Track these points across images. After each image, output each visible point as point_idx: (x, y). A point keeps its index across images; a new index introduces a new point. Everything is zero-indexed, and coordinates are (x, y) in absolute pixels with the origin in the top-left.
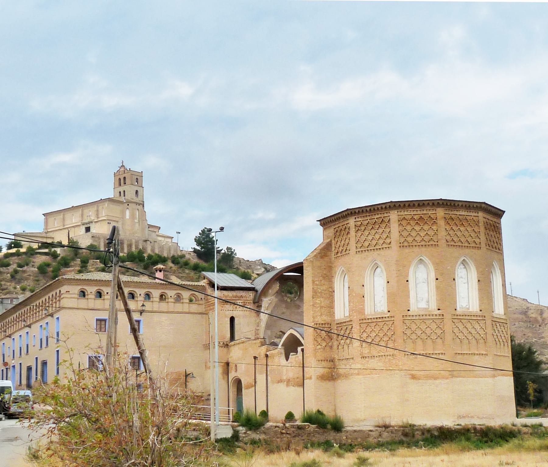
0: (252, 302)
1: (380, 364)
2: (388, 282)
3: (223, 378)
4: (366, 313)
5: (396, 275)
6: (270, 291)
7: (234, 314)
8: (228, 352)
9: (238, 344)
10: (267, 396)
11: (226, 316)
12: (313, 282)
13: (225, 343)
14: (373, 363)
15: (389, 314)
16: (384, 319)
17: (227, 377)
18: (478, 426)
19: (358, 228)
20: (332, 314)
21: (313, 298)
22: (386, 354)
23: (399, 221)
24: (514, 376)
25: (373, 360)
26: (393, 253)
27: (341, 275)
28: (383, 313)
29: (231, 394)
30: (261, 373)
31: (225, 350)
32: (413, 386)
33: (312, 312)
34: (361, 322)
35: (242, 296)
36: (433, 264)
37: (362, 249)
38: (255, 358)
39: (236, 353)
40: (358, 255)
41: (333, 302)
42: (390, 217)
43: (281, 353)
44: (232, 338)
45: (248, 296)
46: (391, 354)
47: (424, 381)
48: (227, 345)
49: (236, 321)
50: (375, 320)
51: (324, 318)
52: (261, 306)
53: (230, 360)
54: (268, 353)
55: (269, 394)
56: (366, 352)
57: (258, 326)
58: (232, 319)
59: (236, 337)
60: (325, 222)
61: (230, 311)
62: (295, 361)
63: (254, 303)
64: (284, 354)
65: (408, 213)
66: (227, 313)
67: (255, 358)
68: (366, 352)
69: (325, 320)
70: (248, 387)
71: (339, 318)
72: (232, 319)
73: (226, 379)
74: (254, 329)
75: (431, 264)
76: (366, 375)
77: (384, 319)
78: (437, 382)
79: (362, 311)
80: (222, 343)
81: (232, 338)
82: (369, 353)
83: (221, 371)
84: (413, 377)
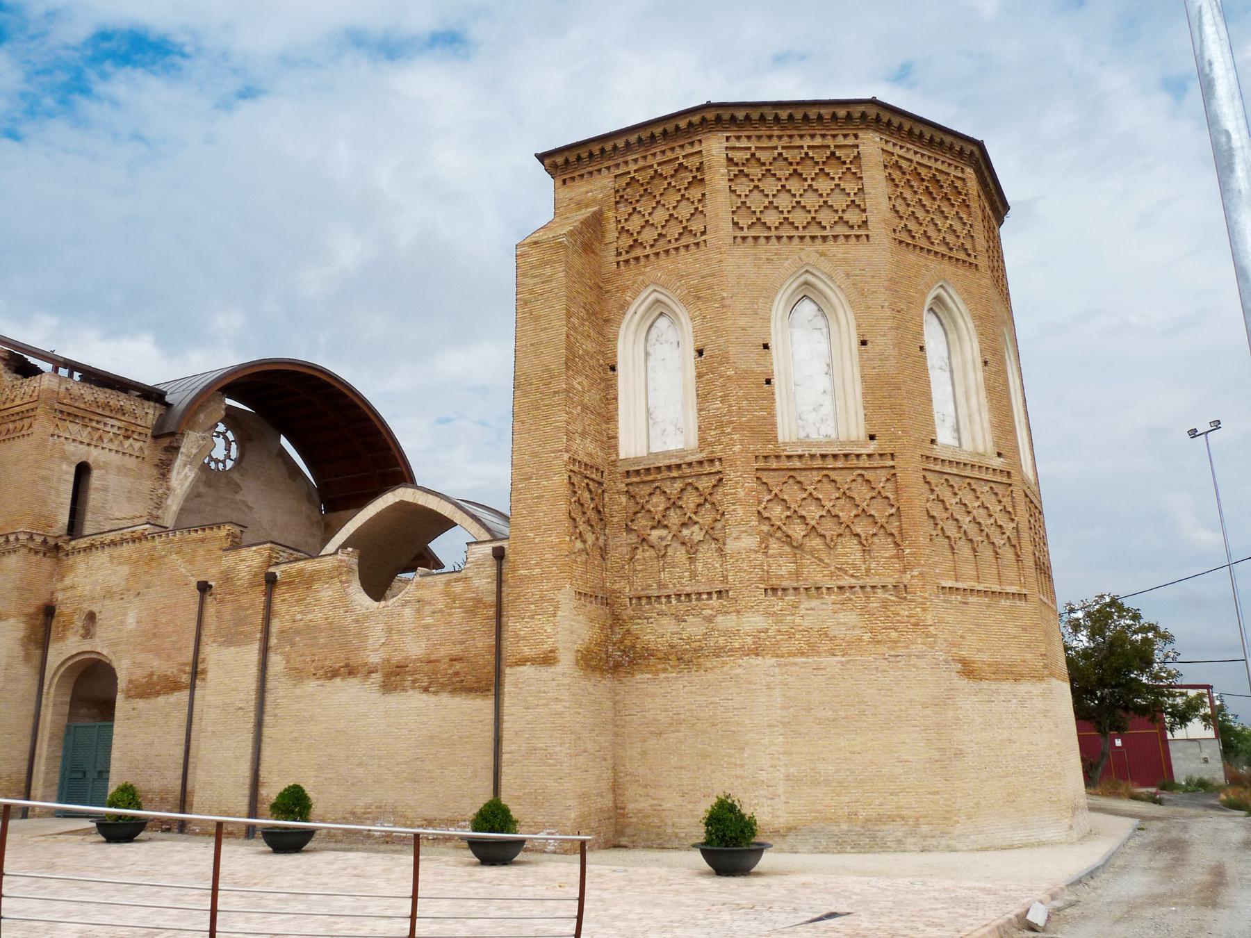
0: (149, 432)
1: (850, 618)
2: (864, 343)
3: (27, 658)
4: (780, 439)
5: (890, 323)
6: (202, 417)
7: (94, 455)
8: (60, 572)
9: (113, 543)
10: (259, 724)
11: (65, 457)
12: (569, 315)
13: (51, 542)
14: (816, 614)
15: (872, 447)
16: (854, 462)
17: (38, 652)
18: (1049, 834)
19: (738, 171)
20: (610, 441)
21: (568, 368)
22: (869, 581)
23: (886, 166)
24: (1072, 681)
25: (814, 603)
26: (878, 253)
27: (642, 317)
28: (855, 443)
29: (48, 715)
30: (231, 639)
31: (47, 563)
32: (970, 700)
33: (564, 417)
34: (761, 464)
35: (122, 410)
36: (974, 317)
37: (753, 229)
38: (204, 587)
39: (91, 577)
40: (740, 250)
41: (609, 398)
42: (861, 148)
43: (350, 570)
44: (74, 527)
45: (139, 412)
46: (890, 581)
47: (994, 686)
48: (57, 548)
49: (95, 479)
50: (818, 463)
51: (591, 447)
52: (177, 449)
53: (60, 596)
54: (277, 571)
55: (268, 719)
56: (784, 571)
57: (158, 506)
58: (83, 471)
59: (89, 527)
60: (564, 162)
61: (76, 445)
62: (447, 593)
63: (156, 437)
64: (357, 574)
65: (910, 153)
66: (70, 447)
67: (204, 587)
68: (784, 571)
69: (590, 455)
70: (149, 689)
71: (641, 452)
72: (83, 471)
73: (36, 661)
74: (145, 513)
75: (968, 318)
76: (791, 654)
77: (854, 462)
78: (1024, 687)
79: (766, 428)
80: (39, 540)
81: (74, 527)
82: (797, 574)
83: (21, 634)
84: (969, 670)
